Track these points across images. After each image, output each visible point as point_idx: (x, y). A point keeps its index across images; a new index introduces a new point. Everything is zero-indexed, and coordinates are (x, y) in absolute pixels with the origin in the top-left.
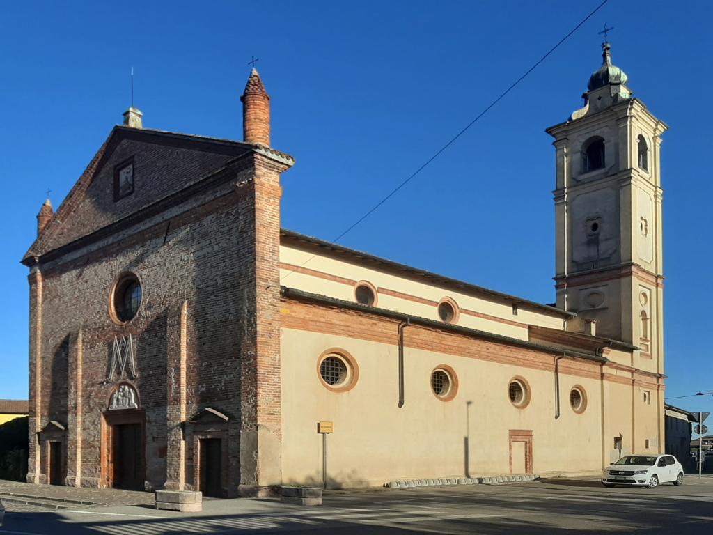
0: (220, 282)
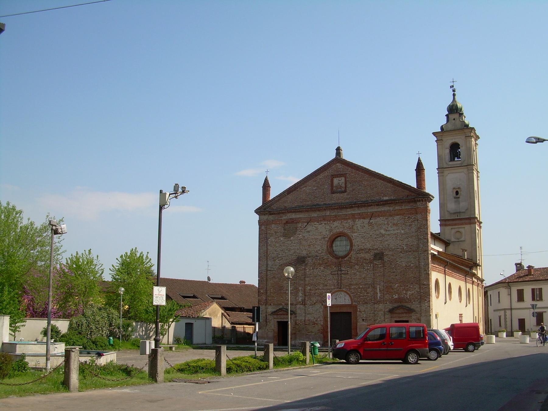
0: (405, 248)
